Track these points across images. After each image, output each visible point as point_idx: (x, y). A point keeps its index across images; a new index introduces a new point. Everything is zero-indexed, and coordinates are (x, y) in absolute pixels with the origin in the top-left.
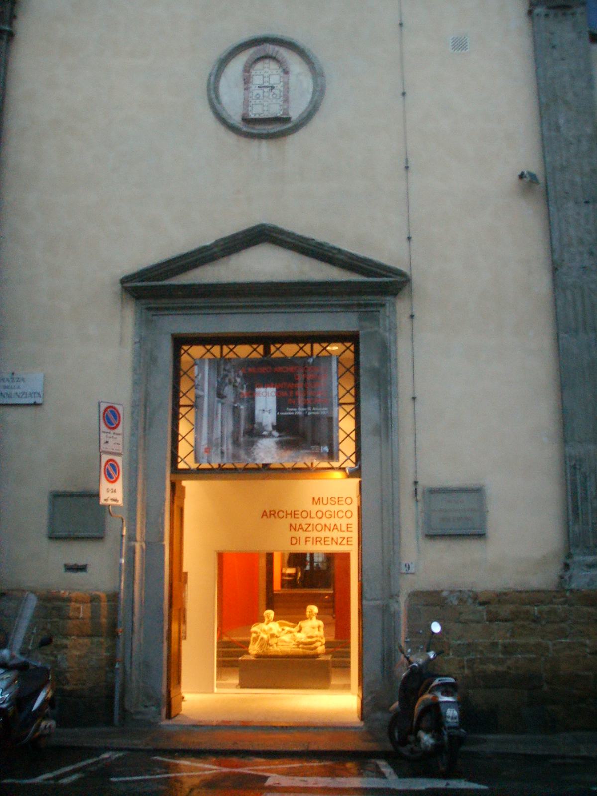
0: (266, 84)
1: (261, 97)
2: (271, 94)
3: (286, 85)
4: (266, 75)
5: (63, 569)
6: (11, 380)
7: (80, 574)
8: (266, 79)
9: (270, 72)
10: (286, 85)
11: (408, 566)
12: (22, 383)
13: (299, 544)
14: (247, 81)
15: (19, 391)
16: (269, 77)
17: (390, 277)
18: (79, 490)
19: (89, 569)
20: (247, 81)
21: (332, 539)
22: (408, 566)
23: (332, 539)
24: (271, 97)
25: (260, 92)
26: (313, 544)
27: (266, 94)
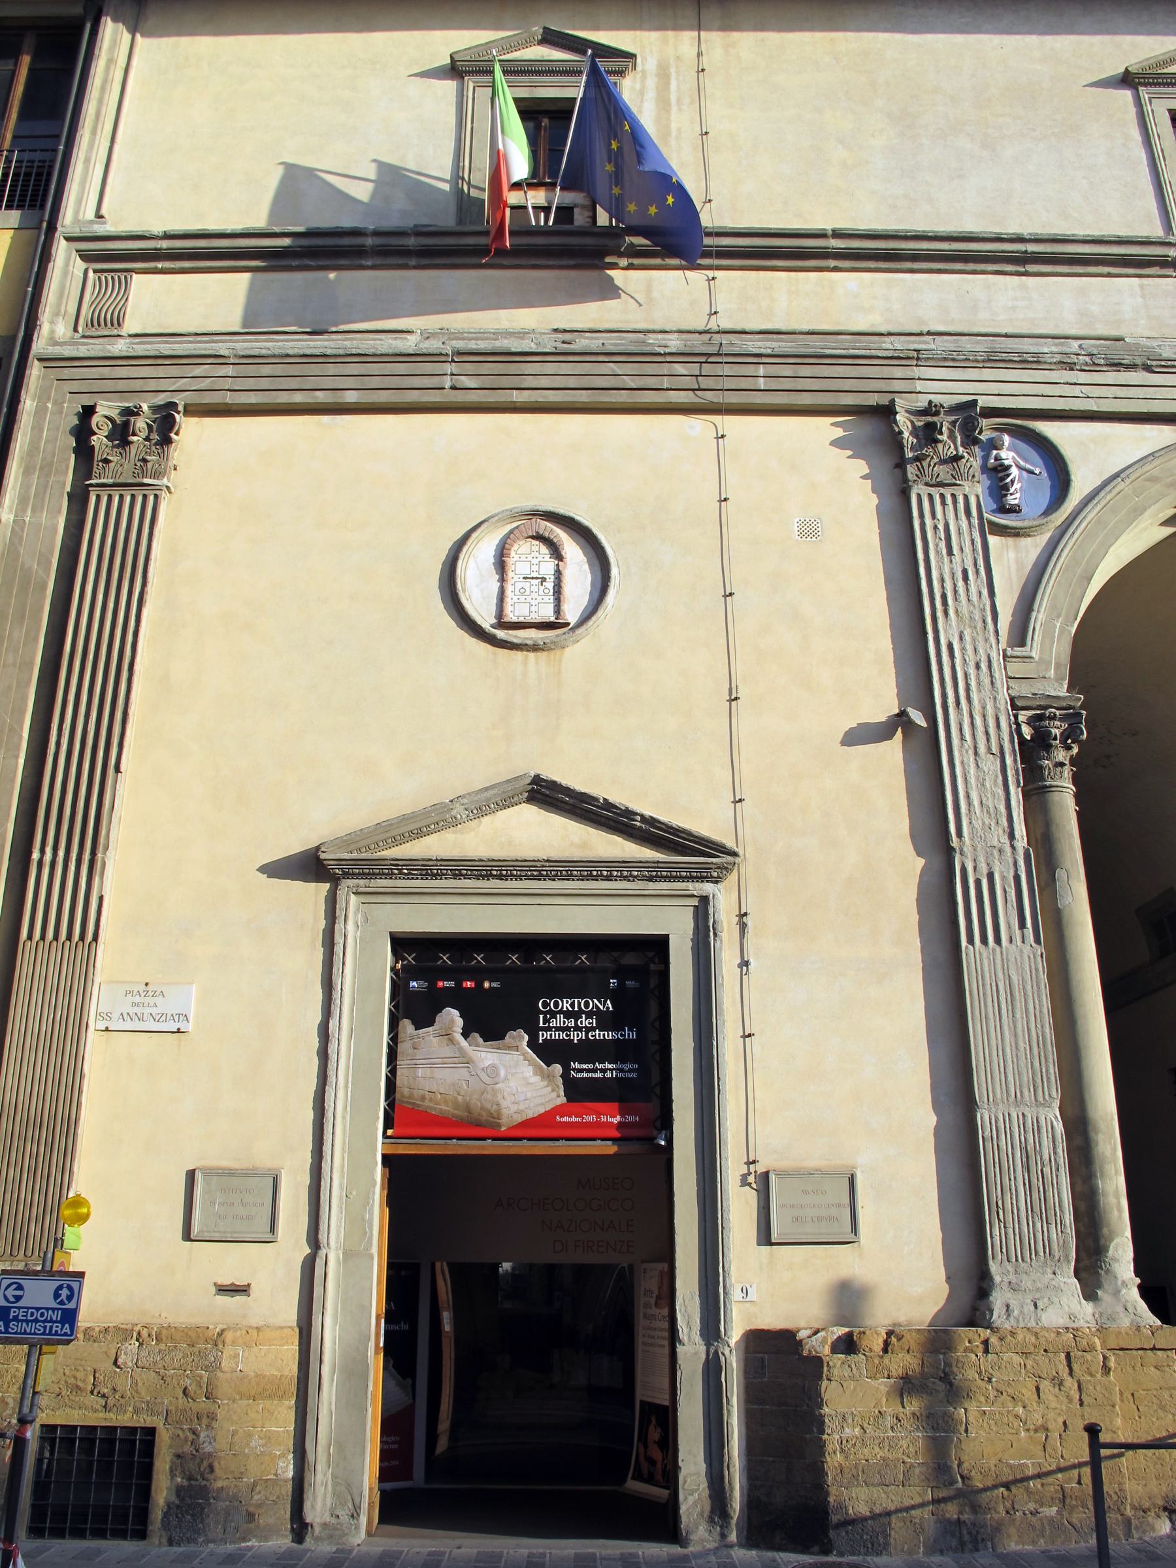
0: (535, 575)
1: (528, 593)
2: (542, 588)
3: (558, 574)
4: (535, 561)
5: (213, 1290)
6: (143, 995)
7: (239, 1299)
8: (535, 568)
9: (540, 559)
10: (558, 574)
11: (744, 1291)
12: (1024, 1276)
13: (567, 1250)
14: (501, 566)
15: (154, 1011)
16: (539, 564)
17: (719, 857)
18: (244, 1166)
19: (254, 1290)
20: (501, 566)
21: (608, 1243)
22: (744, 1291)
23: (608, 1243)
24: (541, 593)
25: (527, 585)
26: (584, 1251)
27: (535, 589)
